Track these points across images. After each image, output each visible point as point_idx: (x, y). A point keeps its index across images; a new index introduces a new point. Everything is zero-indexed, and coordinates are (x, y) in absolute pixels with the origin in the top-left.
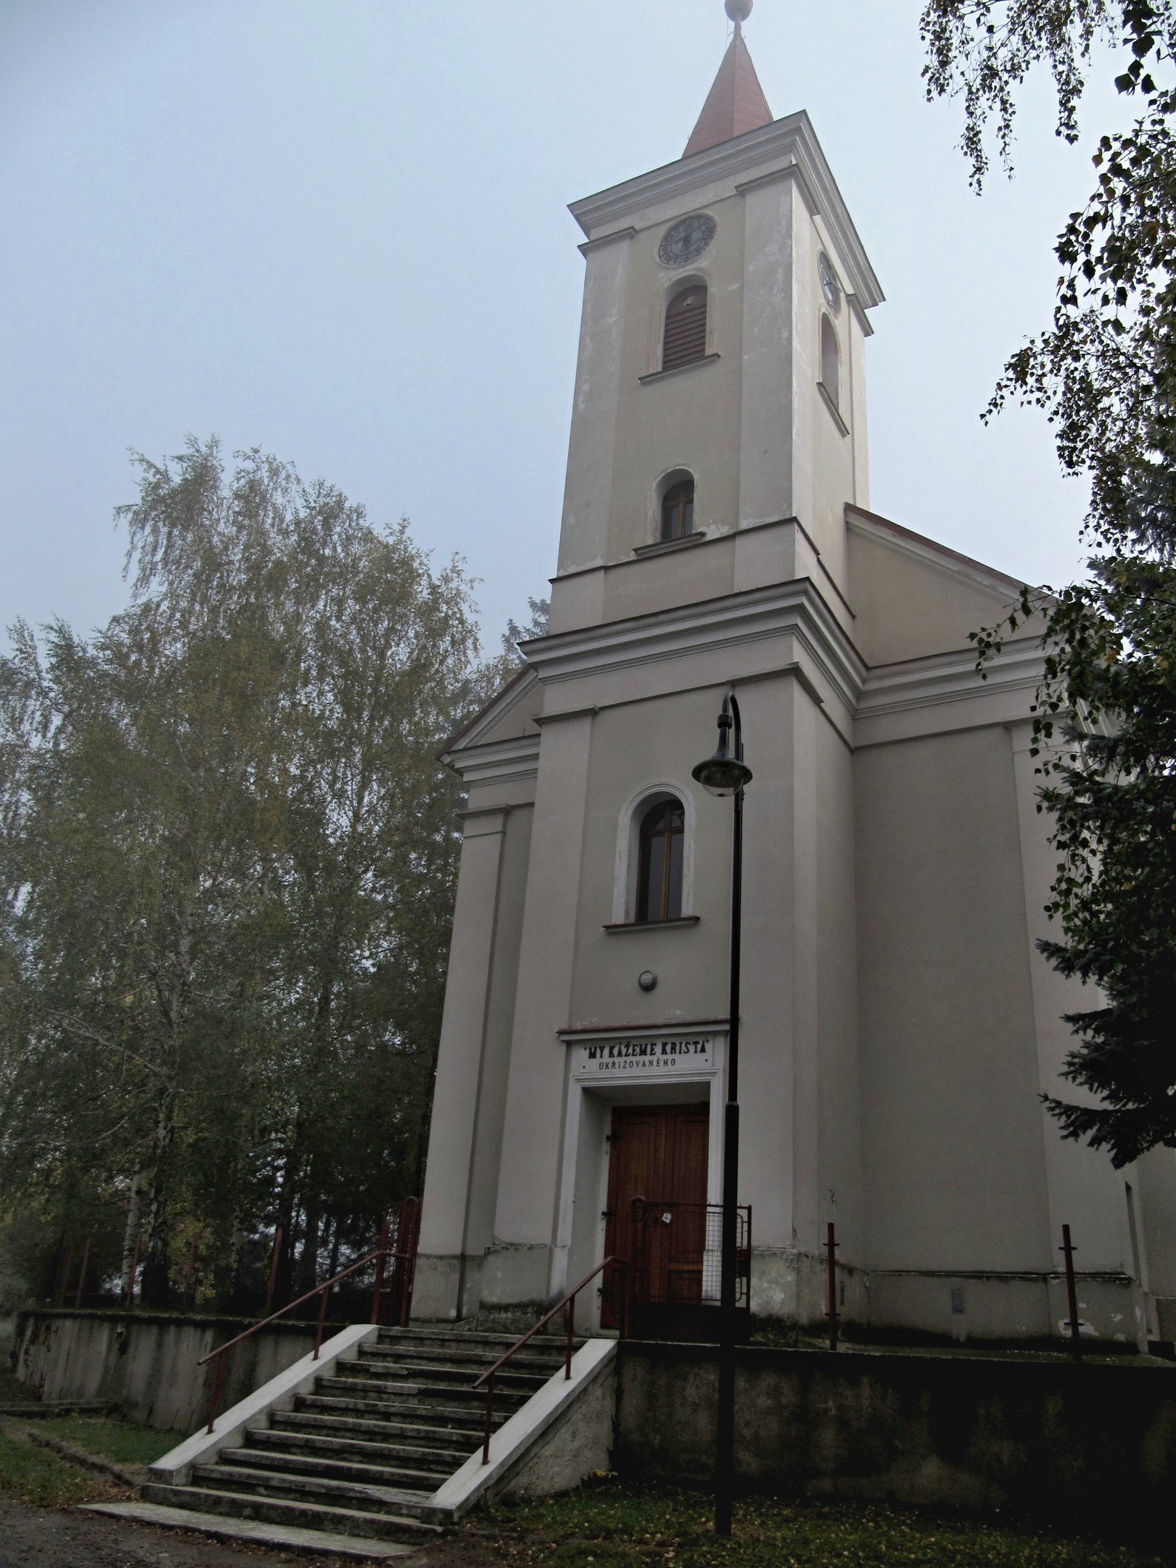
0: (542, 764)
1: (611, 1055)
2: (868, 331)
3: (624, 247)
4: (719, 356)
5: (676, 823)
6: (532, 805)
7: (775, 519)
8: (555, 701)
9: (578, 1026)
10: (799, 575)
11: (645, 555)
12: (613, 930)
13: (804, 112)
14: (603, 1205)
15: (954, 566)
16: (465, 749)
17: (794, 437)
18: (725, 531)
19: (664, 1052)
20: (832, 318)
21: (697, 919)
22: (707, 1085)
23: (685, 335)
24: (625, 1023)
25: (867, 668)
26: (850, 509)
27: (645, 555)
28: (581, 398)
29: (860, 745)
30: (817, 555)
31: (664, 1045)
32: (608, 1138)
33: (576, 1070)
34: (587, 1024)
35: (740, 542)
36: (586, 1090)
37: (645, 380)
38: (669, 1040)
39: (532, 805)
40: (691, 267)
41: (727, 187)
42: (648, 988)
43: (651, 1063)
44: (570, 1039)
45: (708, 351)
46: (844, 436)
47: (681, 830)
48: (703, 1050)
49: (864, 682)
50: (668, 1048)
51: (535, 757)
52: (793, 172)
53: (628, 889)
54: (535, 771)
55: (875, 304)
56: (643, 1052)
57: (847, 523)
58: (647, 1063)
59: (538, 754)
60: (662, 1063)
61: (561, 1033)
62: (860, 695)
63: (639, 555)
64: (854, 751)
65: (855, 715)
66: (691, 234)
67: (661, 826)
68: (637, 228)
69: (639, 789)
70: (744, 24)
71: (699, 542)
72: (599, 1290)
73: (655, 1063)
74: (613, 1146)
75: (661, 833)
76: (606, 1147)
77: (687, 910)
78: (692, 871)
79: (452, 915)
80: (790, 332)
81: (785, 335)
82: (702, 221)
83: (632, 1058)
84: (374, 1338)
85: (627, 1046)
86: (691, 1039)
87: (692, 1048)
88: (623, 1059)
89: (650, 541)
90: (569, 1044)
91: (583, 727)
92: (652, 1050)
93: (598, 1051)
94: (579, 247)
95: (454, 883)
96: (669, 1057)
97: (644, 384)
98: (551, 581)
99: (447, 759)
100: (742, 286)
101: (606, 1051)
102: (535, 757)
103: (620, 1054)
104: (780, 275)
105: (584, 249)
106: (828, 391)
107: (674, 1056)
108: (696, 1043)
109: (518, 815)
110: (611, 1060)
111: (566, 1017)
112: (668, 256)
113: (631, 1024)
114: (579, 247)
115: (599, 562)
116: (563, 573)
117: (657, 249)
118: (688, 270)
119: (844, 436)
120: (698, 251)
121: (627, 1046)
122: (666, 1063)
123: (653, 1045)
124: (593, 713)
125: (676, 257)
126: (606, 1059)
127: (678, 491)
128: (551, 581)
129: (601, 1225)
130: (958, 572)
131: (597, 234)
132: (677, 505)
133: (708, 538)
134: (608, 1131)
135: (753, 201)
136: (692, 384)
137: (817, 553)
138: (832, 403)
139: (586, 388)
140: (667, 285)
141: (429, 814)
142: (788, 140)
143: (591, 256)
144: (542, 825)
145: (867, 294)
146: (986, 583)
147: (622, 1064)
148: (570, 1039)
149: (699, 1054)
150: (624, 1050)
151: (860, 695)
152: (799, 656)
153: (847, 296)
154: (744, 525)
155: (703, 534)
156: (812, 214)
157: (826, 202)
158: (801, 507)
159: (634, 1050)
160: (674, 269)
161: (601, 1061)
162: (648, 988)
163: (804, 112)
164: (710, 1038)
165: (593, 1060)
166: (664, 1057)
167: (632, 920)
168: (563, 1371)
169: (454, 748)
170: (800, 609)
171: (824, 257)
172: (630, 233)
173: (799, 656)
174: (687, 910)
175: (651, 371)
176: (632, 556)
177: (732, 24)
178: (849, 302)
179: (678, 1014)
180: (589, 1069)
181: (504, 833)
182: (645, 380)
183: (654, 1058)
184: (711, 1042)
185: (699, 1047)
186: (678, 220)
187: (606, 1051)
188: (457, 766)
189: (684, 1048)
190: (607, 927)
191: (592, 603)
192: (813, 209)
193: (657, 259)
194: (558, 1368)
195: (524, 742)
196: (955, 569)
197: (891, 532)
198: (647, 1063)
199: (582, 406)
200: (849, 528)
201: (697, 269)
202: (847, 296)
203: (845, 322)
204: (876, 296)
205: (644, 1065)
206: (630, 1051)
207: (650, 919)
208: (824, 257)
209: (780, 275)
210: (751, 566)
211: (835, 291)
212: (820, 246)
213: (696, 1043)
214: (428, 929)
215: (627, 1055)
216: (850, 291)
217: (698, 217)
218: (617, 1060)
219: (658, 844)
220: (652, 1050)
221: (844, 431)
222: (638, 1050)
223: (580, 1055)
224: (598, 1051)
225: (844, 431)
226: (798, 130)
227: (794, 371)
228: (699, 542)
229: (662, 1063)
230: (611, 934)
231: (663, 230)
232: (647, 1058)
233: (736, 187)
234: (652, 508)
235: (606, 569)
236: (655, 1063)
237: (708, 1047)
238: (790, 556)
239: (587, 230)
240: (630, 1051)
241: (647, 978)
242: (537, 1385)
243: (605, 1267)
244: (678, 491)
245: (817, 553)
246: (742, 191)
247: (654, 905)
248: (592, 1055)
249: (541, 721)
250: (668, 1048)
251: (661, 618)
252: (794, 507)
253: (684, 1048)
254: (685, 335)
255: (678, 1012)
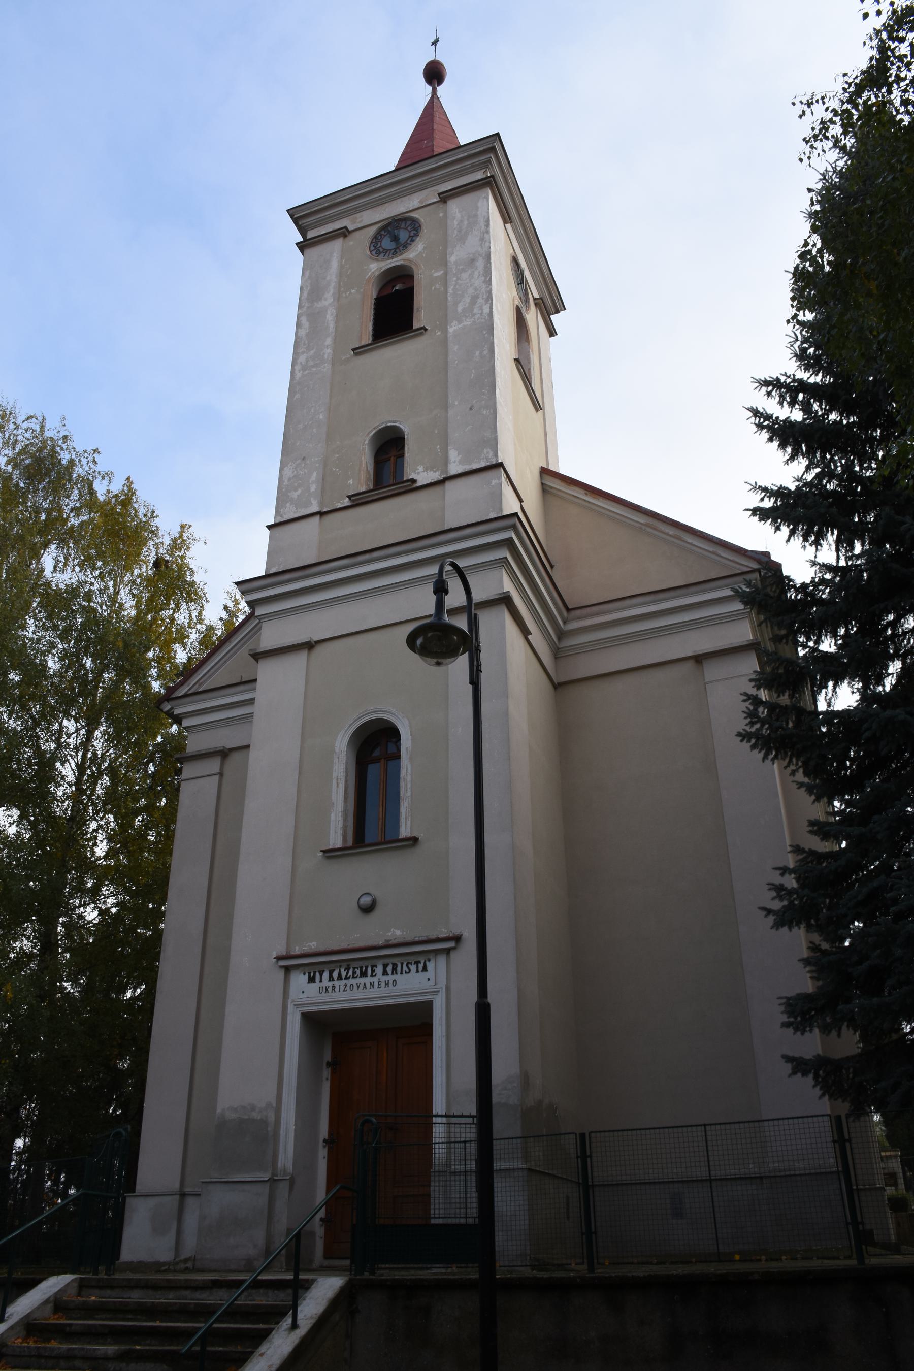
0: (256, 709)
1: (331, 978)
2: (552, 332)
3: (338, 244)
4: (426, 330)
5: (391, 748)
6: (248, 747)
7: (483, 464)
8: (272, 635)
9: (297, 950)
10: (506, 512)
11: (358, 501)
12: (330, 854)
13: (498, 134)
14: (324, 1131)
15: (642, 519)
16: (186, 696)
17: (497, 395)
18: (435, 476)
19: (385, 973)
20: (523, 310)
21: (414, 841)
22: (430, 1004)
23: (395, 312)
24: (344, 945)
25: (568, 610)
26: (545, 472)
27: (358, 501)
28: (297, 367)
29: (563, 680)
30: (521, 496)
31: (385, 966)
32: (328, 1064)
33: (294, 994)
34: (305, 949)
35: (448, 485)
36: (305, 1016)
37: (358, 351)
38: (390, 961)
39: (255, 680)
40: (399, 258)
41: (431, 195)
42: (368, 910)
43: (372, 984)
44: (289, 964)
45: (416, 325)
46: (537, 411)
47: (397, 756)
48: (425, 969)
49: (565, 623)
50: (389, 969)
51: (251, 701)
52: (489, 182)
53: (345, 811)
54: (251, 715)
55: (557, 312)
56: (364, 974)
57: (542, 484)
58: (368, 985)
59: (254, 699)
60: (383, 984)
61: (279, 958)
62: (561, 634)
63: (353, 501)
64: (557, 686)
65: (557, 653)
66: (397, 232)
67: (377, 753)
68: (350, 228)
69: (355, 717)
70: (439, 89)
71: (411, 487)
72: (822, 840)
73: (376, 984)
74: (333, 1073)
75: (377, 760)
76: (326, 1073)
77: (405, 831)
78: (409, 794)
79: (163, 900)
80: (491, 308)
81: (486, 310)
82: (409, 223)
83: (352, 981)
84: (73, 1291)
85: (347, 969)
86: (413, 959)
87: (413, 968)
88: (343, 982)
89: (363, 489)
90: (288, 969)
91: (299, 660)
92: (373, 971)
93: (318, 975)
94: (297, 244)
95: (168, 838)
96: (390, 978)
97: (356, 354)
98: (269, 527)
99: (167, 707)
100: (446, 274)
101: (326, 975)
102: (251, 701)
103: (340, 977)
104: (480, 263)
105: (302, 247)
106: (522, 366)
107: (394, 977)
108: (417, 963)
109: (235, 758)
110: (330, 984)
111: (284, 942)
112: (376, 249)
113: (351, 946)
114: (297, 244)
115: (315, 508)
116: (280, 520)
117: (368, 245)
118: (396, 261)
119: (537, 411)
120: (406, 246)
121: (347, 969)
122: (387, 984)
123: (372, 967)
124: (309, 646)
125: (386, 251)
126: (326, 982)
127: (389, 446)
128: (269, 527)
129: (322, 1153)
130: (647, 525)
131: (310, 234)
132: (389, 459)
133: (419, 484)
134: (328, 1056)
135: (455, 207)
136: (400, 354)
137: (521, 501)
138: (526, 378)
139: (302, 359)
140: (377, 273)
141: (149, 792)
142: (483, 158)
143: (307, 251)
144: (257, 760)
145: (550, 304)
146: (671, 533)
147: (342, 988)
148: (289, 964)
149: (420, 974)
150: (344, 974)
151: (561, 634)
152: (508, 586)
153: (535, 299)
154: (454, 469)
155: (413, 481)
156: (505, 222)
157: (515, 212)
158: (507, 454)
159: (354, 973)
160: (383, 260)
161: (321, 984)
162: (368, 910)
163: (498, 134)
164: (431, 956)
165: (312, 985)
166: (386, 978)
167: (350, 843)
168: (288, 1321)
169: (173, 696)
170: (509, 543)
171: (515, 260)
172: (344, 233)
173: (508, 586)
174: (405, 831)
175: (363, 343)
176: (347, 502)
177: (430, 88)
178: (536, 304)
179: (397, 934)
180: (308, 994)
181: (221, 774)
182: (358, 351)
183: (375, 980)
184: (432, 962)
185: (421, 966)
186: (387, 222)
187: (326, 975)
188: (176, 712)
189: (405, 968)
190: (324, 851)
191: (308, 543)
192: (506, 218)
193: (368, 253)
194: (284, 1314)
195: (241, 688)
196: (642, 521)
197: (584, 492)
198: (368, 985)
199: (298, 375)
200: (545, 490)
201: (404, 260)
202: (535, 299)
203: (532, 317)
204: (559, 307)
205: (365, 987)
206: (351, 973)
207: (367, 841)
208: (515, 260)
209: (480, 263)
210: (461, 504)
211: (526, 293)
212: (512, 251)
213: (417, 963)
214: (145, 877)
215: (346, 978)
216: (537, 296)
217: (405, 220)
218: (337, 983)
219: (374, 771)
220: (373, 971)
221: (537, 406)
222: (358, 972)
223: (299, 980)
224: (318, 975)
225: (537, 406)
226: (493, 149)
227: (495, 341)
228: (411, 487)
229: (383, 984)
230: (328, 857)
231: (374, 229)
232: (368, 980)
233: (439, 194)
234: (364, 459)
235: (321, 514)
236: (376, 984)
237: (430, 966)
238: (498, 497)
239: (302, 230)
240: (351, 973)
241: (366, 900)
242: (262, 1337)
243: (327, 1203)
244: (389, 446)
245: (521, 501)
246: (444, 198)
247: (372, 825)
248: (312, 980)
249: (257, 656)
250: (389, 969)
251: (375, 554)
252: (500, 454)
253: (405, 968)
254: (395, 312)
255: (398, 933)
